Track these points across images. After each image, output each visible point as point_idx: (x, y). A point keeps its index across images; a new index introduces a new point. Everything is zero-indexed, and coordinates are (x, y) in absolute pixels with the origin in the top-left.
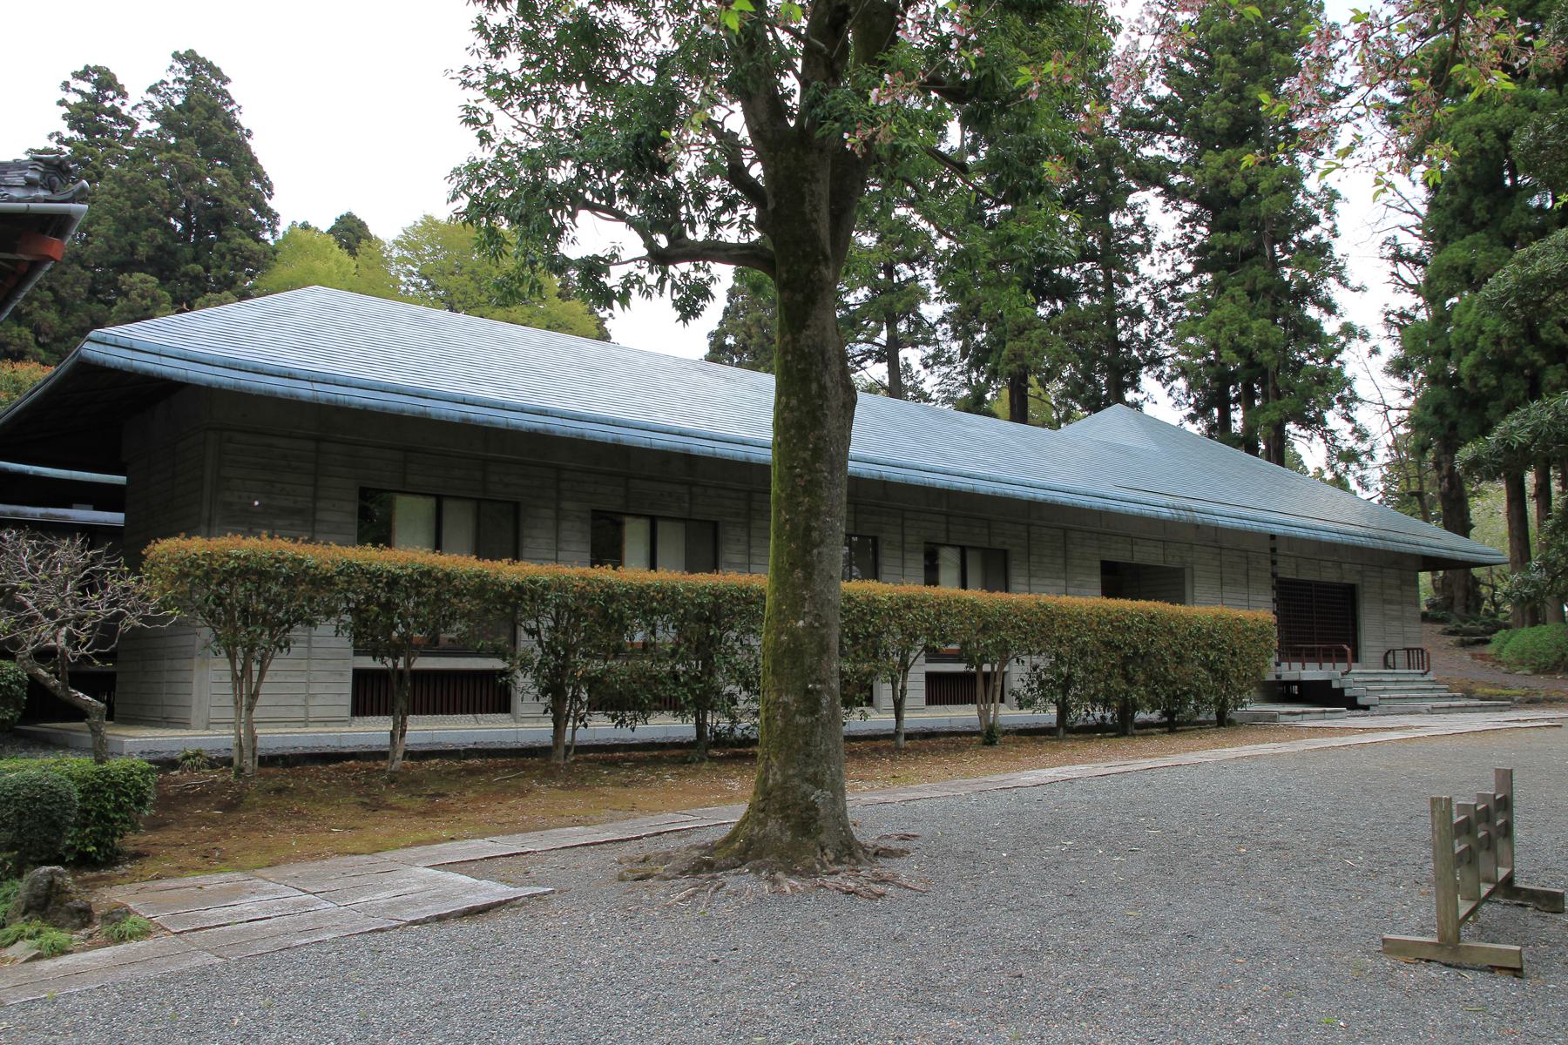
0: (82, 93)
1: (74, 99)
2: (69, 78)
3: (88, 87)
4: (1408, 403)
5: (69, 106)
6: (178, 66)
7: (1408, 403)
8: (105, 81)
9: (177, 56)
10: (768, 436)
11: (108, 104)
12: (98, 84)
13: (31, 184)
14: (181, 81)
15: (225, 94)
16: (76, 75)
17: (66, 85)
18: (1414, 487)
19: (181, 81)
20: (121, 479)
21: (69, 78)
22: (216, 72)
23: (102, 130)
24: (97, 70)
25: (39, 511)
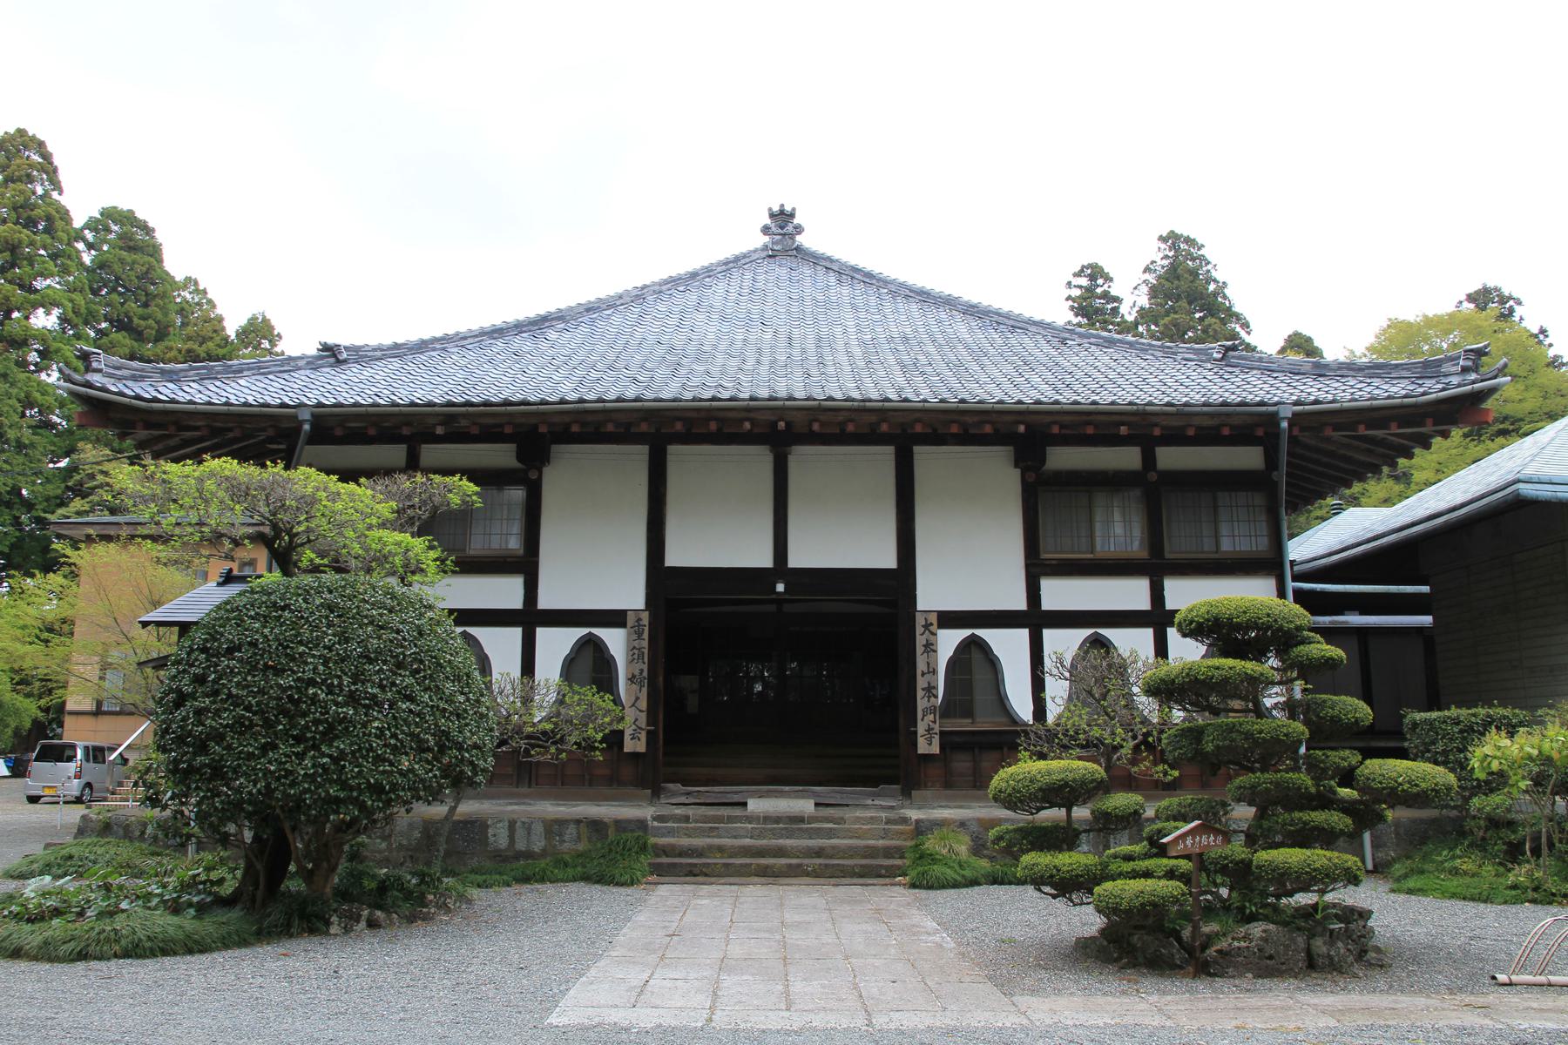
0: (1080, 287)
1: (1076, 293)
2: (1071, 278)
3: (1084, 282)
4: (1166, 262)
5: (1074, 300)
6: (1163, 246)
7: (1166, 262)
8: (1095, 273)
9: (1162, 239)
10: (472, 553)
11: (1099, 290)
12: (1092, 278)
13: (1465, 370)
14: (1166, 257)
15: (1202, 258)
16: (1077, 275)
17: (1069, 283)
18: (77, 734)
19: (1166, 257)
20: (1425, 589)
21: (1071, 278)
22: (1189, 241)
23: (1098, 311)
24: (1090, 266)
25: (1327, 619)
